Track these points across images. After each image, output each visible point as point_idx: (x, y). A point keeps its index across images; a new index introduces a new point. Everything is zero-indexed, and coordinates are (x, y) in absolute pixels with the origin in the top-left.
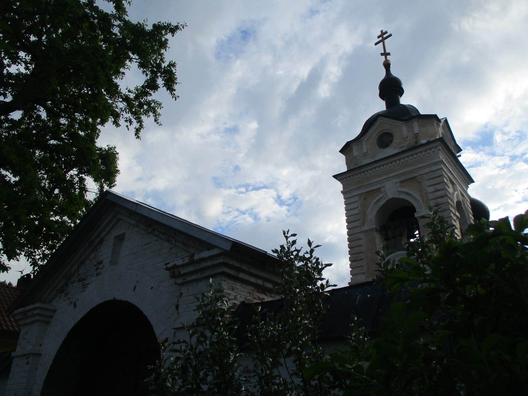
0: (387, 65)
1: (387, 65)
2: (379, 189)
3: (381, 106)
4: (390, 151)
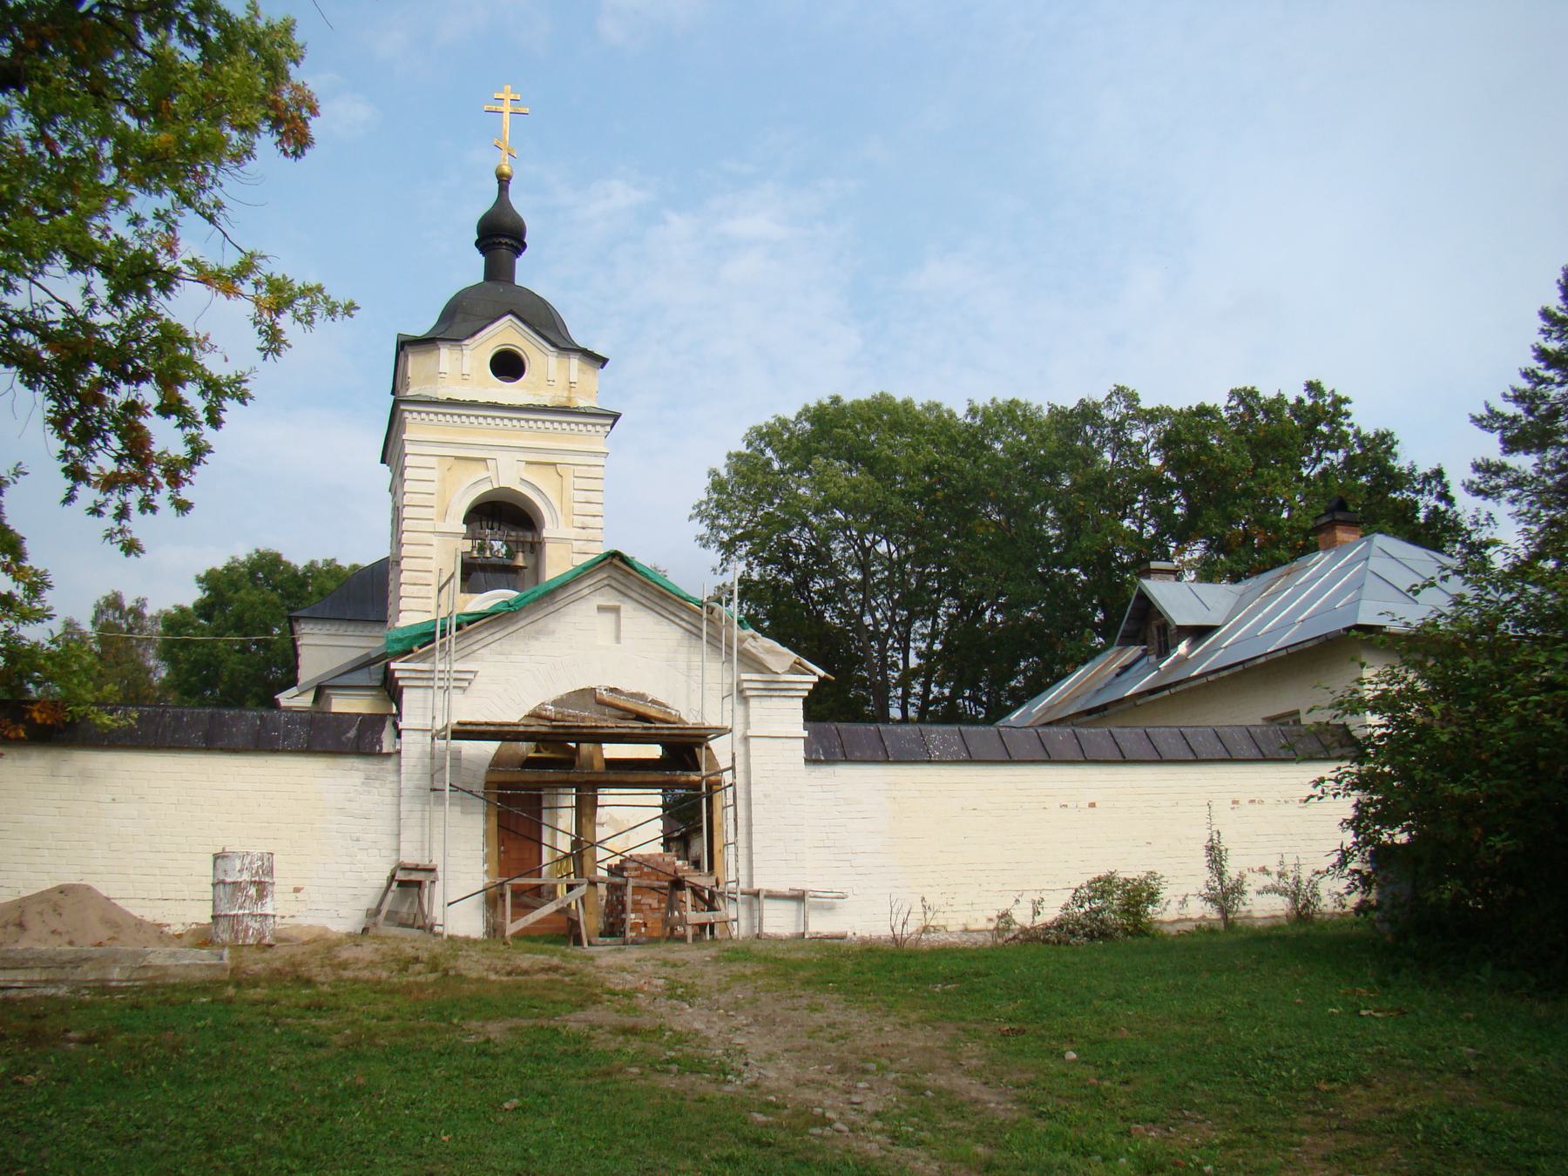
0: (503, 181)
1: (503, 181)
2: (484, 460)
3: (471, 269)
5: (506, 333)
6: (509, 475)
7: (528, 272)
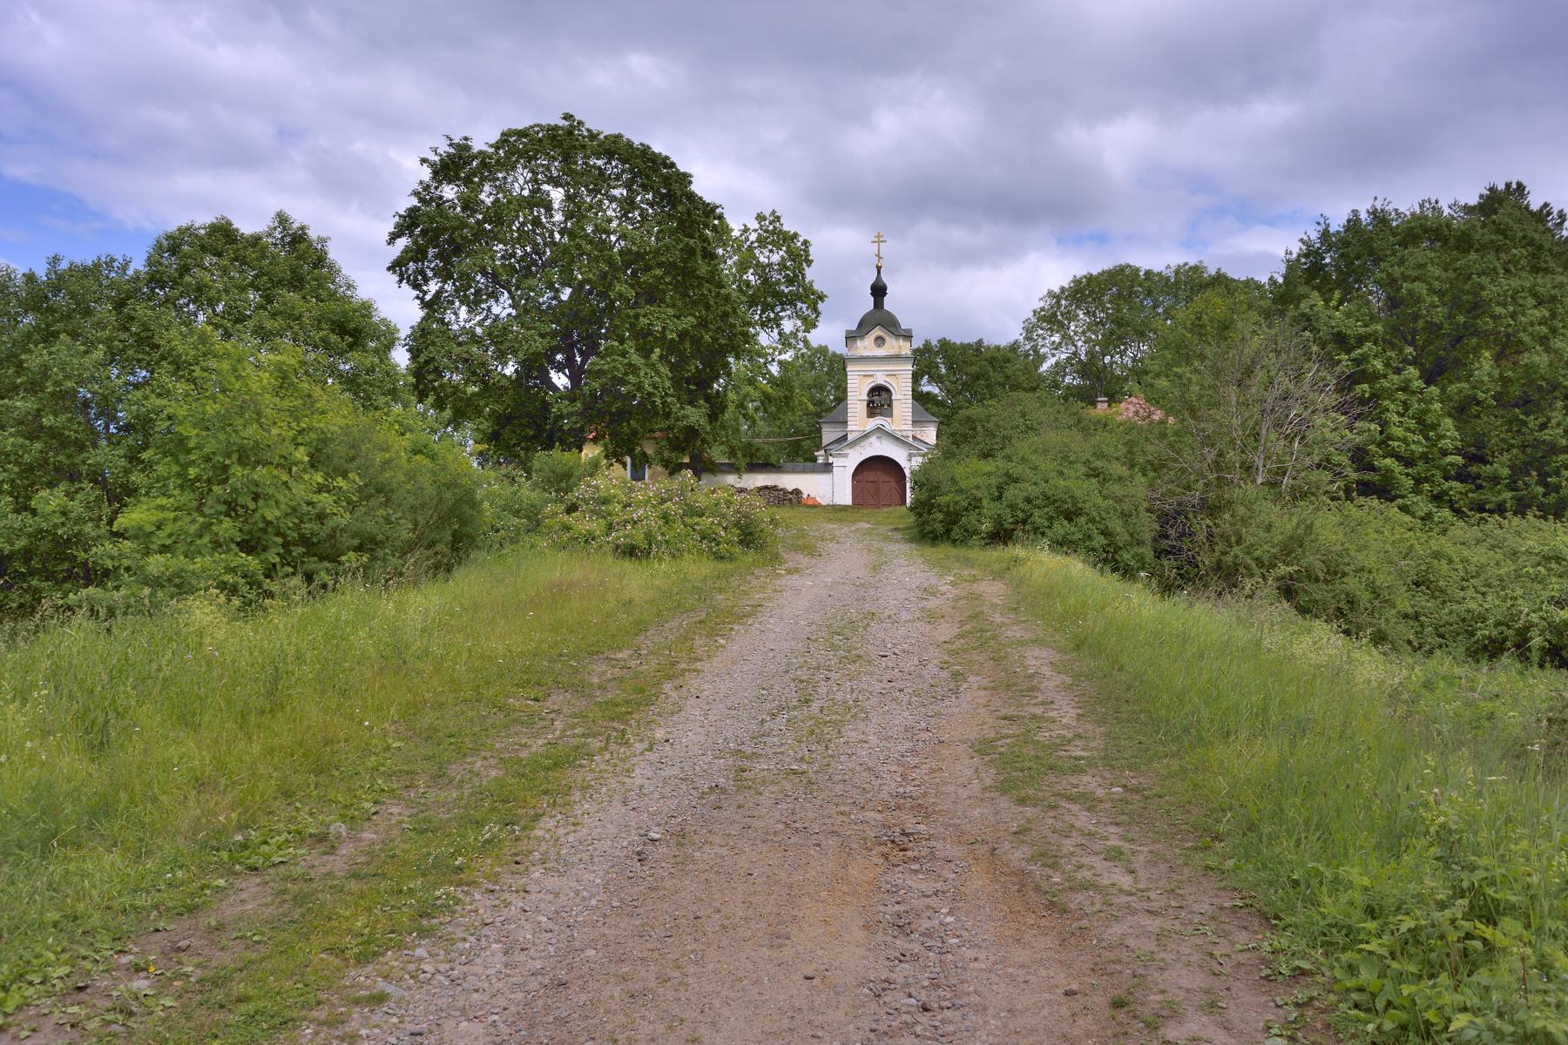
0: (879, 269)
1: (879, 269)
3: (869, 303)
4: (881, 352)
5: (878, 332)
6: (881, 380)
7: (889, 303)
